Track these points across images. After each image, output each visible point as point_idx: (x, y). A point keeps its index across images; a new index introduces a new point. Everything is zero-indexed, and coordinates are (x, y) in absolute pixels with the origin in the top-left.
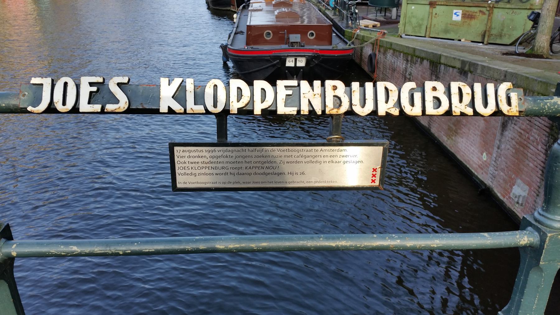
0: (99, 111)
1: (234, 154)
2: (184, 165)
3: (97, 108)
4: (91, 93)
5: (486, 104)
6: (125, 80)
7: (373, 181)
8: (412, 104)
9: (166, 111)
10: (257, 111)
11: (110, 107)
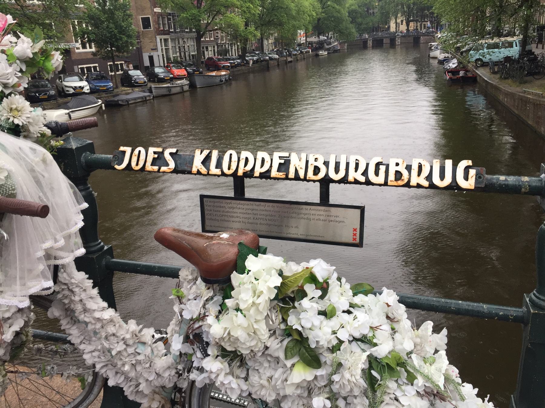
0: (383, 183)
1: (245, 207)
2: (210, 212)
3: (156, 168)
4: (154, 159)
5: (442, 176)
6: (174, 150)
7: (355, 239)
8: (377, 173)
9: (353, 181)
10: (257, 174)
11: (163, 169)
